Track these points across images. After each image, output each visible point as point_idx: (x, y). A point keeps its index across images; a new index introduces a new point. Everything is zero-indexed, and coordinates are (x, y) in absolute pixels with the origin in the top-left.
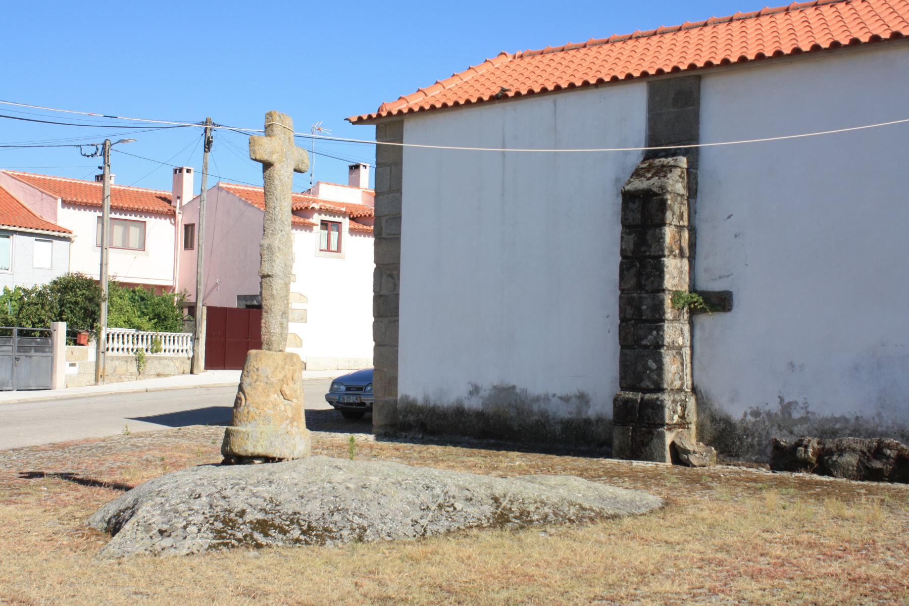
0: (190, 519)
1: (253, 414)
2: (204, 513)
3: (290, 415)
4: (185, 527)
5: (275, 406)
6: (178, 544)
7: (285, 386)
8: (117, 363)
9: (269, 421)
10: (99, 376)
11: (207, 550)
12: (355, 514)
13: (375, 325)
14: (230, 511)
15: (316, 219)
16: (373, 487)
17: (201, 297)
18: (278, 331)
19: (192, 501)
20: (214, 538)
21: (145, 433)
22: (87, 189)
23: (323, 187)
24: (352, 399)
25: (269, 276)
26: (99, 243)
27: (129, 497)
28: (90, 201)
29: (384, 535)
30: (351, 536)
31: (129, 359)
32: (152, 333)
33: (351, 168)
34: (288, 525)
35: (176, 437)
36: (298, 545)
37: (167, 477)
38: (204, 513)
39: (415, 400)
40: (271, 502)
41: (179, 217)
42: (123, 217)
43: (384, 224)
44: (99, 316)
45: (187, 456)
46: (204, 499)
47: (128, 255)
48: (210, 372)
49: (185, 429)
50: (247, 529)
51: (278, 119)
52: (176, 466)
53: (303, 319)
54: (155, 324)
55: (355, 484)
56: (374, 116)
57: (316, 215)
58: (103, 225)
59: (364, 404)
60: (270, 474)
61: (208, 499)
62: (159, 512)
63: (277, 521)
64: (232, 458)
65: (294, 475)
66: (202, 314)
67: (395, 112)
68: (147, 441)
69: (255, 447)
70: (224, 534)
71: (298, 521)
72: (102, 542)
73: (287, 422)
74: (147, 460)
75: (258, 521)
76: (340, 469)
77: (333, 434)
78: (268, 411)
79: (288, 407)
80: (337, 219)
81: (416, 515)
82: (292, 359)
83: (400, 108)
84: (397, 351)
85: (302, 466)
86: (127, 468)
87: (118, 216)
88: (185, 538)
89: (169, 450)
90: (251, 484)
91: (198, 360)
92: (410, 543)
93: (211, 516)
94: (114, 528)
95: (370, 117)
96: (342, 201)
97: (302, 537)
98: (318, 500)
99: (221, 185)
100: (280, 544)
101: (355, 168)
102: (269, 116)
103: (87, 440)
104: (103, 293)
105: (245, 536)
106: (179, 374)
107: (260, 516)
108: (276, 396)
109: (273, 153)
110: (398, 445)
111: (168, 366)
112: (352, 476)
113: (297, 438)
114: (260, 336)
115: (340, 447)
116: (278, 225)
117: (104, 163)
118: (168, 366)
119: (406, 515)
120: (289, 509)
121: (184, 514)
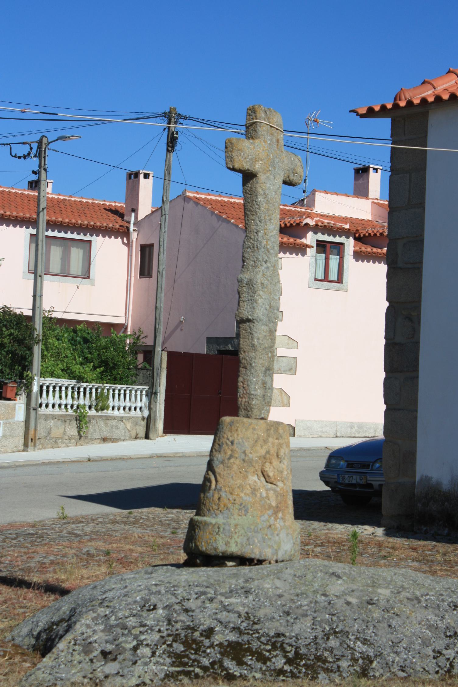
0: (142, 637)
1: (226, 501)
2: (159, 631)
3: (274, 504)
4: (135, 649)
5: (254, 490)
6: (126, 671)
7: (267, 465)
8: (52, 423)
9: (247, 511)
10: (29, 440)
11: (162, 680)
12: (357, 639)
13: (386, 382)
14: (194, 629)
15: (310, 239)
16: (383, 603)
17: (160, 339)
18: (259, 392)
19: (144, 614)
20: (173, 664)
21: (86, 517)
22: (18, 199)
23: (319, 197)
24: (355, 479)
25: (249, 320)
26: (32, 268)
27: (65, 605)
28: (21, 214)
29: (395, 669)
30: (351, 669)
31: (68, 419)
32: (97, 385)
33: (357, 171)
34: (269, 651)
35: (125, 523)
36: (282, 678)
37: (113, 580)
38: (159, 631)
39: (439, 484)
40: (248, 618)
41: (134, 236)
42: (62, 235)
43: (400, 245)
44: (31, 362)
45: (140, 549)
46: (160, 611)
47: (68, 286)
48: (170, 437)
49: (136, 512)
50: (214, 654)
51: (263, 115)
52: (126, 562)
53: (292, 370)
54: (101, 373)
55: (358, 598)
56: (389, 106)
57: (310, 234)
58: (37, 246)
59: (370, 486)
60: (246, 581)
61: (166, 612)
62: (102, 627)
63: (255, 645)
64: (198, 557)
65: (278, 583)
66: (161, 360)
67: (416, 101)
68: (89, 529)
69: (227, 544)
70: (186, 660)
71: (282, 646)
72: (28, 665)
73: (270, 512)
74: (88, 554)
75: (230, 644)
76: (339, 577)
77: (330, 525)
78: (245, 498)
79: (271, 493)
80: (337, 239)
81: (440, 644)
82: (277, 430)
83: (423, 95)
84: (416, 418)
85: (289, 571)
86: (63, 564)
87: (56, 234)
88: (135, 663)
89: (117, 541)
90: (221, 594)
91: (155, 420)
92: (430, 682)
93: (169, 635)
94: (45, 645)
95: (383, 107)
96: (344, 215)
97: (287, 668)
98: (309, 618)
99: (188, 194)
100: (258, 675)
101: (362, 172)
102: (252, 111)
103: (12, 525)
104: (36, 333)
105: (213, 664)
106: (131, 438)
107: (233, 637)
108: (255, 478)
109: (255, 160)
110: (416, 543)
111: (117, 428)
112: (355, 587)
113: (283, 535)
114: (236, 399)
115: (337, 543)
116: (261, 255)
117: (40, 166)
118: (117, 428)
119: (426, 643)
120: (270, 628)
121: (134, 632)
